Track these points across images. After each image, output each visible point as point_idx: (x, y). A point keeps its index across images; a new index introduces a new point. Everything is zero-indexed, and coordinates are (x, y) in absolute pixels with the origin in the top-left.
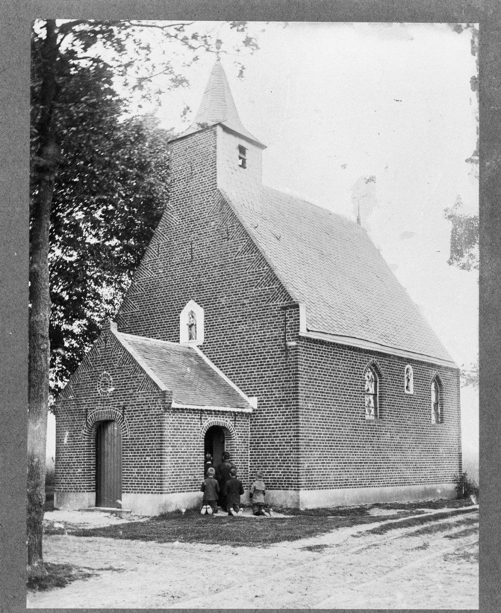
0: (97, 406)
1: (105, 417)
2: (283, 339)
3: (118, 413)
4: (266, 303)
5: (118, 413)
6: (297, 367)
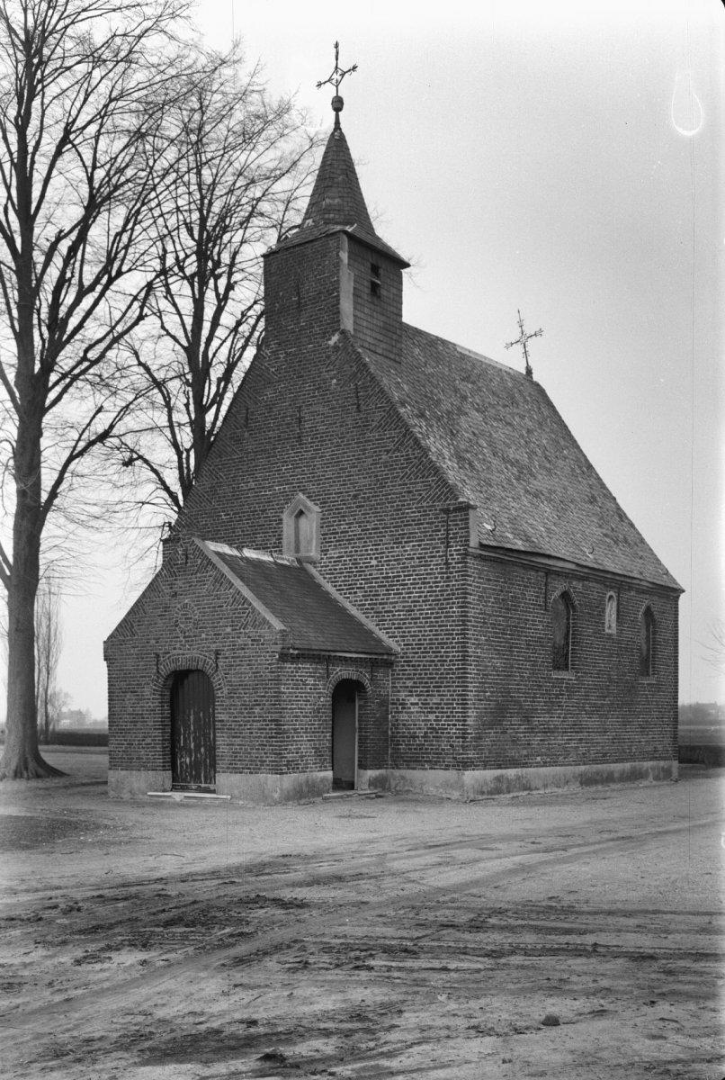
0: (175, 649)
1: (183, 664)
2: (442, 556)
3: (208, 660)
4: (418, 503)
5: (208, 660)
6: (466, 598)
